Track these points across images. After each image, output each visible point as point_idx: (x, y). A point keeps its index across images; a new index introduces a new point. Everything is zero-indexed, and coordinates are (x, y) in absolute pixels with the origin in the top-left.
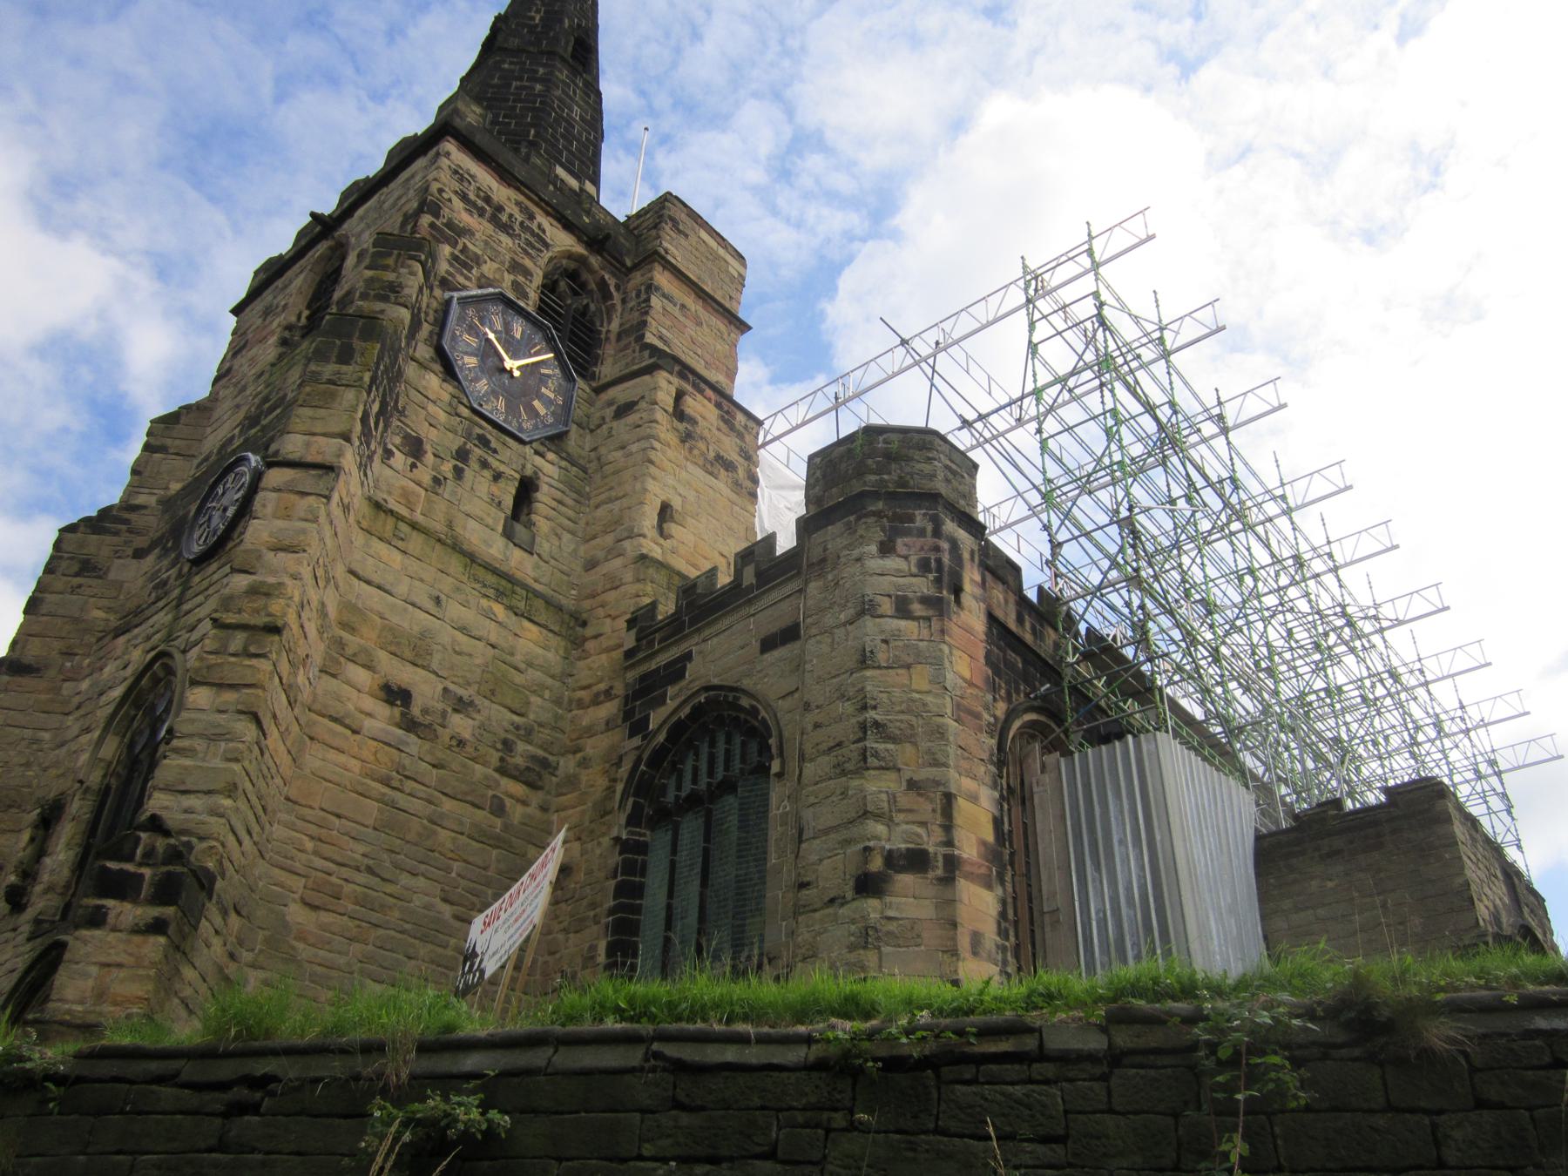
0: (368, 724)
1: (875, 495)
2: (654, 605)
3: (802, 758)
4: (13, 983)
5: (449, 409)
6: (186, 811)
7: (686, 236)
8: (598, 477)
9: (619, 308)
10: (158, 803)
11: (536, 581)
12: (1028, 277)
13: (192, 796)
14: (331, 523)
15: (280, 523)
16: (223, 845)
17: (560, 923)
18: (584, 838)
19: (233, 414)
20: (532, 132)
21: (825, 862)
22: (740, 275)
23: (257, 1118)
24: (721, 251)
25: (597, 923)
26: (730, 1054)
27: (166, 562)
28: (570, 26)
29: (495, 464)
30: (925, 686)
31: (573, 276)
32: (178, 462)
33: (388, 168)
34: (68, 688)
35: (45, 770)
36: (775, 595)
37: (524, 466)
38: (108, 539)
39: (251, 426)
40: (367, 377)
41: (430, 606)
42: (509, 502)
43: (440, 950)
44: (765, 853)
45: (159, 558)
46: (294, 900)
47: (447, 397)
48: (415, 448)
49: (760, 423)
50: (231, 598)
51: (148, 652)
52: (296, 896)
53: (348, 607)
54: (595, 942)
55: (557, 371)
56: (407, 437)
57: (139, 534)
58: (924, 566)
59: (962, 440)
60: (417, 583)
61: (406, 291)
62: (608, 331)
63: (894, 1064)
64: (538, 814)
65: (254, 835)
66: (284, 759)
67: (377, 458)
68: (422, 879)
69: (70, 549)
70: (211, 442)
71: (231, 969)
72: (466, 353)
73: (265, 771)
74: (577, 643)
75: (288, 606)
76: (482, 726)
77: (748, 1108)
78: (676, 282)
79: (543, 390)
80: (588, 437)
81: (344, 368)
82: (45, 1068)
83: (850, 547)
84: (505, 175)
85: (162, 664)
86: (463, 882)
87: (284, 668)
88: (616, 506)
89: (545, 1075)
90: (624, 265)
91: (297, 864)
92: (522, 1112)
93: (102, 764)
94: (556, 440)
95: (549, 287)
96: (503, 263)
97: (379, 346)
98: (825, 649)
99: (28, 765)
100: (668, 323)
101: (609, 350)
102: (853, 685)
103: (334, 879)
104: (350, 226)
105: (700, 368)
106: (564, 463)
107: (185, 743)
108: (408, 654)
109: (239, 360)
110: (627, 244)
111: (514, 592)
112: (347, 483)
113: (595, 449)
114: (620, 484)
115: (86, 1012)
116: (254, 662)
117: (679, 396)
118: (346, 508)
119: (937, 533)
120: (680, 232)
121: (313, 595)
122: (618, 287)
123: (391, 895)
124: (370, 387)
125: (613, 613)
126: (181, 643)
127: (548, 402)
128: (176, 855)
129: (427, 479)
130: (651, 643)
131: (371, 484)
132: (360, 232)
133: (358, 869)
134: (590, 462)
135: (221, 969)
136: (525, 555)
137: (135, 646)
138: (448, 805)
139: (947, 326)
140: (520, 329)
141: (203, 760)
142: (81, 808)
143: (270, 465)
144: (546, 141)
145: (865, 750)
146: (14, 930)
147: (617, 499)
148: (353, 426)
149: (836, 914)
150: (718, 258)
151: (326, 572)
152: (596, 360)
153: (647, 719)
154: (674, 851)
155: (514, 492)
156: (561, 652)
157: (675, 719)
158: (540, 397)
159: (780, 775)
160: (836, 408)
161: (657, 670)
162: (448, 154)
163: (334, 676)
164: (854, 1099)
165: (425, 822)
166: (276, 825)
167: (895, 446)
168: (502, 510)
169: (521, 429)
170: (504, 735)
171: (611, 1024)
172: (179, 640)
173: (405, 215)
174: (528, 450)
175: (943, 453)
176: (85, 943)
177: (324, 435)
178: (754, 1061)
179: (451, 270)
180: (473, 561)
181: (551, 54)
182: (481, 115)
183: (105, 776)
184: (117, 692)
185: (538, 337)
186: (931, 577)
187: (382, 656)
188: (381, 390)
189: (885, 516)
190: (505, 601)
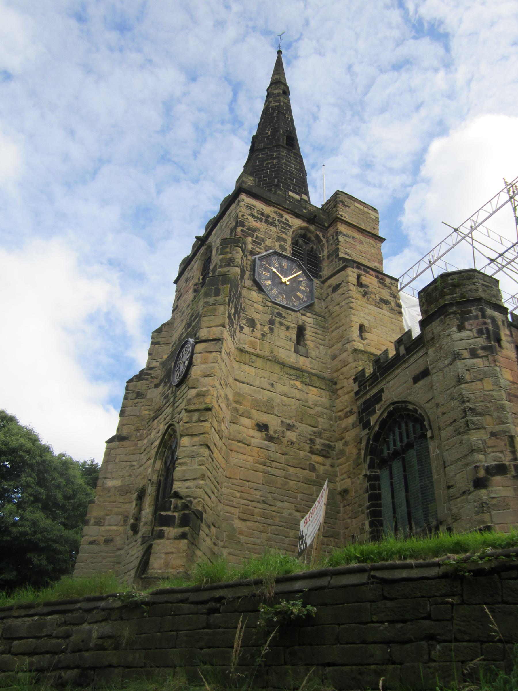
0: (253, 441)
1: (451, 305)
2: (363, 370)
3: (439, 429)
4: (139, 562)
5: (263, 304)
6: (187, 488)
7: (349, 207)
8: (330, 319)
9: (326, 245)
10: (177, 486)
11: (312, 369)
12: (508, 187)
13: (189, 481)
14: (224, 362)
15: (204, 366)
16: (203, 500)
17: (348, 515)
18: (351, 476)
19: (181, 324)
20: (276, 180)
21: (458, 475)
22: (376, 217)
23: (219, 614)
24: (366, 210)
25: (363, 513)
26: (404, 574)
27: (166, 388)
28: (283, 132)
29: (286, 323)
30: (491, 388)
31: (304, 236)
32: (165, 347)
33: (221, 211)
34: (140, 443)
35: (137, 477)
36: (415, 357)
37: (298, 321)
38: (145, 382)
39: (189, 328)
40: (227, 300)
41: (269, 388)
42: (294, 337)
44: (431, 474)
45: (164, 386)
46: (236, 518)
47: (261, 300)
48: (252, 323)
49: (397, 280)
50: (190, 399)
51: (166, 425)
52: (236, 516)
53: (237, 394)
54: (364, 522)
55: (305, 278)
56: (248, 319)
57: (155, 378)
58: (480, 332)
59: (489, 272)
60: (263, 379)
61: (237, 260)
62: (323, 256)
63: (479, 573)
64: (330, 469)
65: (215, 494)
66: (222, 461)
67: (237, 331)
68: (286, 503)
69: (132, 389)
70: (175, 337)
71: (216, 549)
72: (266, 280)
73: (215, 467)
74: (334, 392)
75: (212, 399)
76: (300, 435)
77: (416, 597)
78: (348, 228)
79: (300, 287)
80: (323, 303)
81: (218, 298)
82: (141, 600)
83: (444, 330)
84: (267, 202)
85: (172, 429)
86: (304, 502)
87: (215, 424)
88: (340, 330)
89: (329, 588)
90: (324, 226)
91: (234, 503)
92: (321, 605)
93: (156, 472)
94: (310, 307)
95: (295, 243)
96: (273, 239)
97: (229, 286)
98: (441, 378)
99: (130, 476)
100: (348, 246)
101: (325, 264)
102: (457, 393)
103: (250, 507)
104: (211, 239)
105: (366, 262)
106: (315, 316)
108: (264, 409)
109: (180, 301)
110: (324, 217)
112: (227, 344)
113: (326, 308)
114: (340, 321)
115: (163, 573)
116: (203, 424)
117: (359, 277)
118: (229, 354)
119: (484, 316)
120: (346, 206)
121: (222, 393)
122: (324, 236)
123: (274, 511)
124: (229, 303)
125: (347, 377)
126: (176, 419)
127: (303, 292)
128: (186, 507)
129: (259, 335)
130: (365, 387)
131: (237, 342)
132: (215, 240)
133: (259, 502)
134: (326, 313)
135: (211, 550)
136: (305, 359)
137: (161, 423)
138: (291, 470)
139: (474, 218)
140: (286, 264)
141: (190, 466)
142: (151, 490)
143: (196, 343)
144: (282, 182)
145: (467, 421)
146: (136, 541)
147: (340, 327)
148: (225, 321)
149: (467, 499)
150: (364, 213)
151: (225, 382)
152: (320, 269)
153: (369, 420)
154: (391, 477)
155: (296, 333)
156: (328, 397)
157: (381, 419)
158: (299, 290)
159: (432, 438)
160: (430, 266)
161: (370, 398)
162: (243, 200)
163: (236, 423)
164: (462, 590)
165: (283, 478)
166: (223, 488)
167: (456, 281)
168: (292, 342)
169: (294, 306)
170: (310, 437)
171: (354, 564)
172: (176, 418)
173: (231, 229)
174: (299, 314)
175: (480, 279)
176: (158, 545)
177: (215, 326)
178: (415, 576)
179: (253, 247)
180: (284, 366)
181: (278, 146)
182: (253, 180)
183: (158, 476)
184: (157, 443)
185: (294, 266)
186: (484, 337)
187: (254, 412)
188: (234, 303)
189: (458, 313)
190: (300, 380)
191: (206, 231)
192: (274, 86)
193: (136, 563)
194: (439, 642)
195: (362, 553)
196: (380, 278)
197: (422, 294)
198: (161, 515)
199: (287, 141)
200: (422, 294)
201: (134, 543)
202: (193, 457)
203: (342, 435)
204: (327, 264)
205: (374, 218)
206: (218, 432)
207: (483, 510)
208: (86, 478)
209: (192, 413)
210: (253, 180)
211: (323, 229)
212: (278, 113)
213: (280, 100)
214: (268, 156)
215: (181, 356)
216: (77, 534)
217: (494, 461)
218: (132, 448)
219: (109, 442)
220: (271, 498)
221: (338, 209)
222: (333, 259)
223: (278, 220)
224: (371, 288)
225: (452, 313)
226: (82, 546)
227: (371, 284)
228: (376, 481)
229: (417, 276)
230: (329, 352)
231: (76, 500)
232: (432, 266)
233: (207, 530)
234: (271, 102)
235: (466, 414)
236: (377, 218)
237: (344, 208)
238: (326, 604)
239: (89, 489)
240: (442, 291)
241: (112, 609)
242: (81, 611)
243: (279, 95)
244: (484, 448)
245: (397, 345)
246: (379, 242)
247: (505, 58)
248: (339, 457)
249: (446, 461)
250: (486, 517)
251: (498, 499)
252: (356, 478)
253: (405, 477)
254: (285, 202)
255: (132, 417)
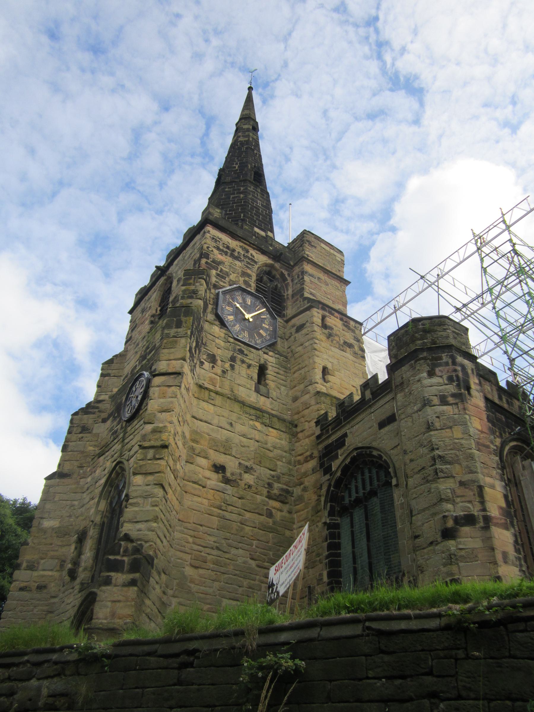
0: (209, 482)
1: (422, 350)
2: (326, 414)
5: (224, 340)
7: (315, 247)
8: (292, 359)
9: (291, 284)
10: (127, 528)
12: (476, 238)
13: (140, 524)
14: (182, 397)
16: (155, 544)
20: (242, 215)
21: (426, 525)
22: (342, 260)
24: (332, 251)
25: (321, 563)
26: (403, 625)
27: (115, 423)
28: (251, 167)
29: (247, 361)
30: (460, 436)
31: (269, 273)
32: (115, 379)
33: (185, 242)
34: (82, 482)
35: (77, 517)
36: (381, 402)
37: (260, 360)
38: (92, 416)
39: (143, 360)
40: (189, 332)
41: (228, 427)
42: (255, 376)
43: (252, 582)
45: (113, 421)
46: (187, 565)
47: (223, 335)
48: (213, 359)
49: (361, 324)
51: (113, 462)
52: (188, 563)
53: (194, 432)
55: (268, 316)
56: (209, 355)
57: (103, 412)
58: (450, 380)
60: (222, 418)
61: (200, 293)
62: (288, 295)
63: (484, 624)
64: (287, 515)
65: (167, 538)
66: (175, 503)
67: (197, 366)
68: (240, 550)
69: (77, 422)
70: (128, 369)
71: (165, 598)
72: (229, 315)
73: (169, 509)
74: (294, 435)
75: (169, 435)
76: (258, 478)
77: (415, 651)
78: (314, 268)
79: (263, 325)
80: (286, 343)
81: (179, 330)
82: (101, 652)
83: (414, 375)
84: (233, 236)
85: (120, 467)
86: (259, 550)
87: (171, 462)
88: (302, 371)
89: (319, 641)
90: (289, 264)
91: (187, 549)
92: (310, 659)
93: (100, 513)
94: (272, 346)
95: (259, 280)
96: (238, 273)
97: (192, 318)
98: (410, 424)
99: (70, 516)
100: (313, 287)
101: (289, 303)
102: (426, 439)
103: (203, 554)
105: (330, 304)
106: (277, 356)
107: (134, 501)
108: (222, 450)
109: (135, 333)
110: (290, 256)
111: (263, 416)
113: (289, 347)
114: (303, 361)
116: (159, 462)
117: (323, 318)
118: (188, 390)
119: (454, 363)
120: (312, 246)
121: (179, 429)
122: (289, 275)
123: (228, 559)
127: (266, 330)
129: (219, 372)
130: (327, 431)
133: (212, 548)
136: (266, 399)
138: (248, 515)
139: (441, 266)
140: (250, 300)
145: (436, 469)
146: (73, 588)
147: (303, 368)
148: (186, 354)
150: (331, 254)
152: (284, 308)
153: (331, 465)
154: (352, 526)
155: (257, 371)
156: (288, 440)
157: (344, 464)
158: (262, 328)
159: (397, 486)
160: (395, 312)
162: (209, 232)
163: (192, 463)
165: (239, 524)
166: (176, 532)
167: (427, 326)
168: (253, 380)
169: (256, 344)
170: (268, 481)
171: (344, 615)
172: (125, 456)
173: (195, 260)
174: (261, 352)
176: (104, 592)
177: (175, 360)
178: (415, 628)
179: (217, 280)
181: (245, 181)
182: (220, 213)
183: (101, 518)
184: (103, 481)
185: (258, 303)
186: (455, 384)
187: (211, 452)
188: (195, 336)
189: (429, 359)
191: (166, 261)
192: (243, 121)
193: (72, 612)
194: (442, 700)
195: (351, 603)
196: (345, 320)
197: (392, 338)
198: (109, 560)
199: (254, 177)
200: (392, 338)
201: (71, 591)
202: (146, 497)
203: (302, 480)
204: (291, 303)
205: (340, 260)
206: (174, 471)
207: (451, 562)
208: (17, 518)
209: (147, 450)
210: (220, 213)
211: (288, 267)
212: (247, 148)
213: (248, 136)
214: (234, 190)
215: (134, 389)
216: (4, 579)
217: (463, 511)
218: (73, 486)
219: (48, 478)
220: (225, 545)
221: (304, 248)
222: (298, 298)
223: (244, 255)
224: (336, 330)
225: (422, 358)
226: (11, 593)
227: (336, 326)
228: (336, 529)
229: (381, 321)
230: (290, 393)
231: (4, 542)
232: (397, 312)
233: (157, 577)
234: (239, 137)
235: (435, 461)
236: (343, 261)
237: (310, 248)
238: (315, 658)
239: (19, 529)
240: (413, 335)
241: (67, 662)
242: (29, 665)
243: (248, 130)
244: (453, 497)
245: (363, 389)
246: (344, 285)
247: (476, 117)
248: (297, 503)
249: (413, 509)
250: (454, 568)
251: (467, 550)
252: (315, 525)
253: (367, 526)
254: (252, 238)
255: (76, 453)
